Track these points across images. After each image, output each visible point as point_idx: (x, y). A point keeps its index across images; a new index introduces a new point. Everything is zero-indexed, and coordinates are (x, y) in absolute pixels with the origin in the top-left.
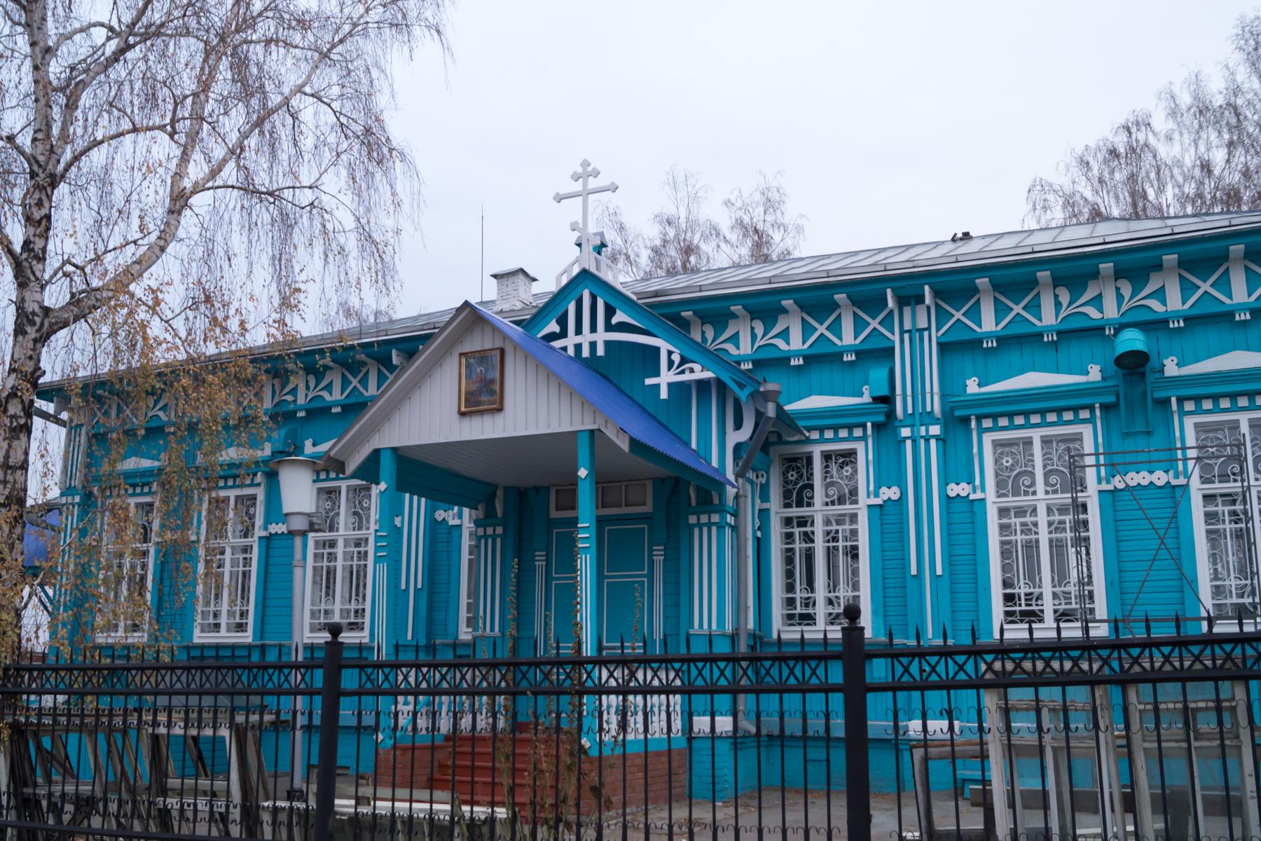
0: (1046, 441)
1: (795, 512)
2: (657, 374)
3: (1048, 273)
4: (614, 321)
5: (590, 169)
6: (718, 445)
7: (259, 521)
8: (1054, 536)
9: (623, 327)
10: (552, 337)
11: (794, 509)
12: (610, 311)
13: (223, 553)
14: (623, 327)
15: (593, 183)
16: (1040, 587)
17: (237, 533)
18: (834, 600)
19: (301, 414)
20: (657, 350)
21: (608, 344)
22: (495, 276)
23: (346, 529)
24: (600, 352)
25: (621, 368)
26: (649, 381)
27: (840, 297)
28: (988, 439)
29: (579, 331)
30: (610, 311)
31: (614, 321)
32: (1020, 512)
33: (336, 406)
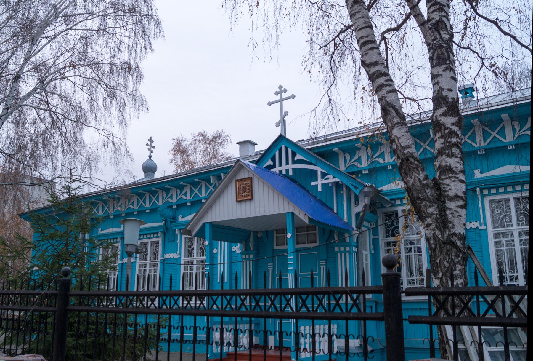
0: (517, 199)
1: (391, 239)
2: (317, 180)
3: (507, 115)
4: (296, 159)
5: (283, 89)
6: (348, 212)
7: (160, 253)
8: (523, 247)
9: (300, 162)
10: (269, 167)
11: (391, 238)
12: (294, 154)
13: (145, 267)
14: (300, 162)
15: (284, 95)
16: (517, 272)
17: (199, 254)
18: (411, 281)
19: (135, 213)
20: (316, 172)
21: (294, 170)
22: (238, 143)
23: (197, 256)
24: (291, 174)
25: (299, 181)
26: (313, 184)
27: (475, 121)
28: (487, 200)
29: (281, 165)
30: (294, 154)
31: (296, 159)
32: (505, 235)
33: (174, 205)
